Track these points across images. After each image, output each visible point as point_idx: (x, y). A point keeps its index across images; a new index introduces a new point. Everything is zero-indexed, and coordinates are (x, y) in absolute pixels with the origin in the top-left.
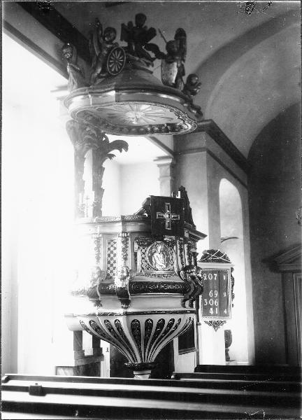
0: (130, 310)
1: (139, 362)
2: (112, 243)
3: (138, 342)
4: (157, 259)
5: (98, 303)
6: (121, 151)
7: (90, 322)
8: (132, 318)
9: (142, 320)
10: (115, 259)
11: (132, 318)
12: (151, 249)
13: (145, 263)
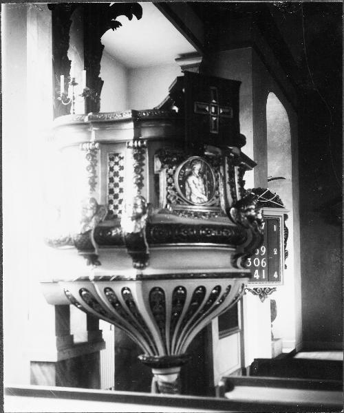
0: (148, 271)
1: (162, 354)
2: (117, 159)
3: (160, 323)
4: (192, 186)
5: (94, 260)
6: (130, 18)
7: (81, 291)
8: (151, 285)
9: (168, 287)
10: (121, 185)
11: (151, 285)
12: (184, 168)
13: (173, 193)
